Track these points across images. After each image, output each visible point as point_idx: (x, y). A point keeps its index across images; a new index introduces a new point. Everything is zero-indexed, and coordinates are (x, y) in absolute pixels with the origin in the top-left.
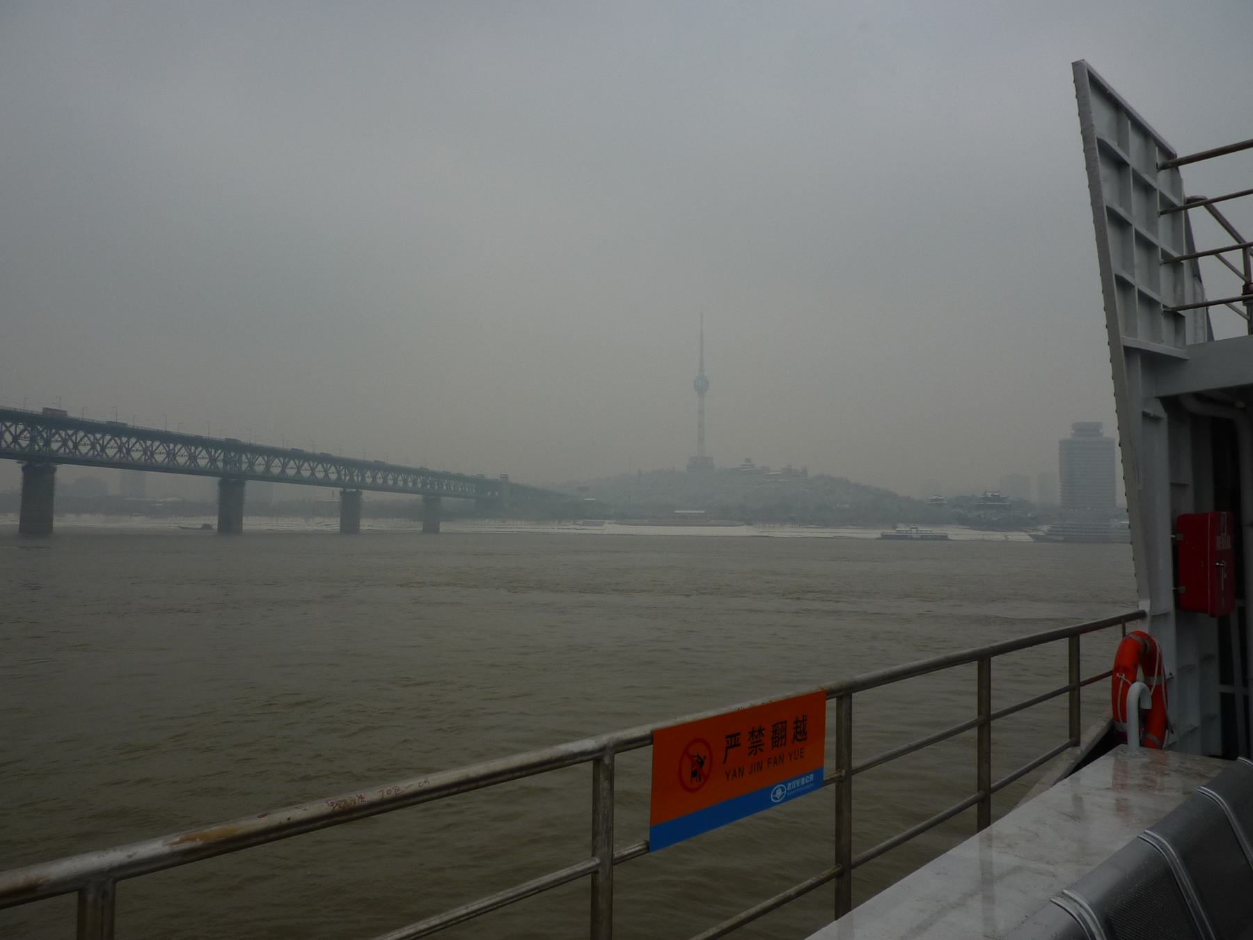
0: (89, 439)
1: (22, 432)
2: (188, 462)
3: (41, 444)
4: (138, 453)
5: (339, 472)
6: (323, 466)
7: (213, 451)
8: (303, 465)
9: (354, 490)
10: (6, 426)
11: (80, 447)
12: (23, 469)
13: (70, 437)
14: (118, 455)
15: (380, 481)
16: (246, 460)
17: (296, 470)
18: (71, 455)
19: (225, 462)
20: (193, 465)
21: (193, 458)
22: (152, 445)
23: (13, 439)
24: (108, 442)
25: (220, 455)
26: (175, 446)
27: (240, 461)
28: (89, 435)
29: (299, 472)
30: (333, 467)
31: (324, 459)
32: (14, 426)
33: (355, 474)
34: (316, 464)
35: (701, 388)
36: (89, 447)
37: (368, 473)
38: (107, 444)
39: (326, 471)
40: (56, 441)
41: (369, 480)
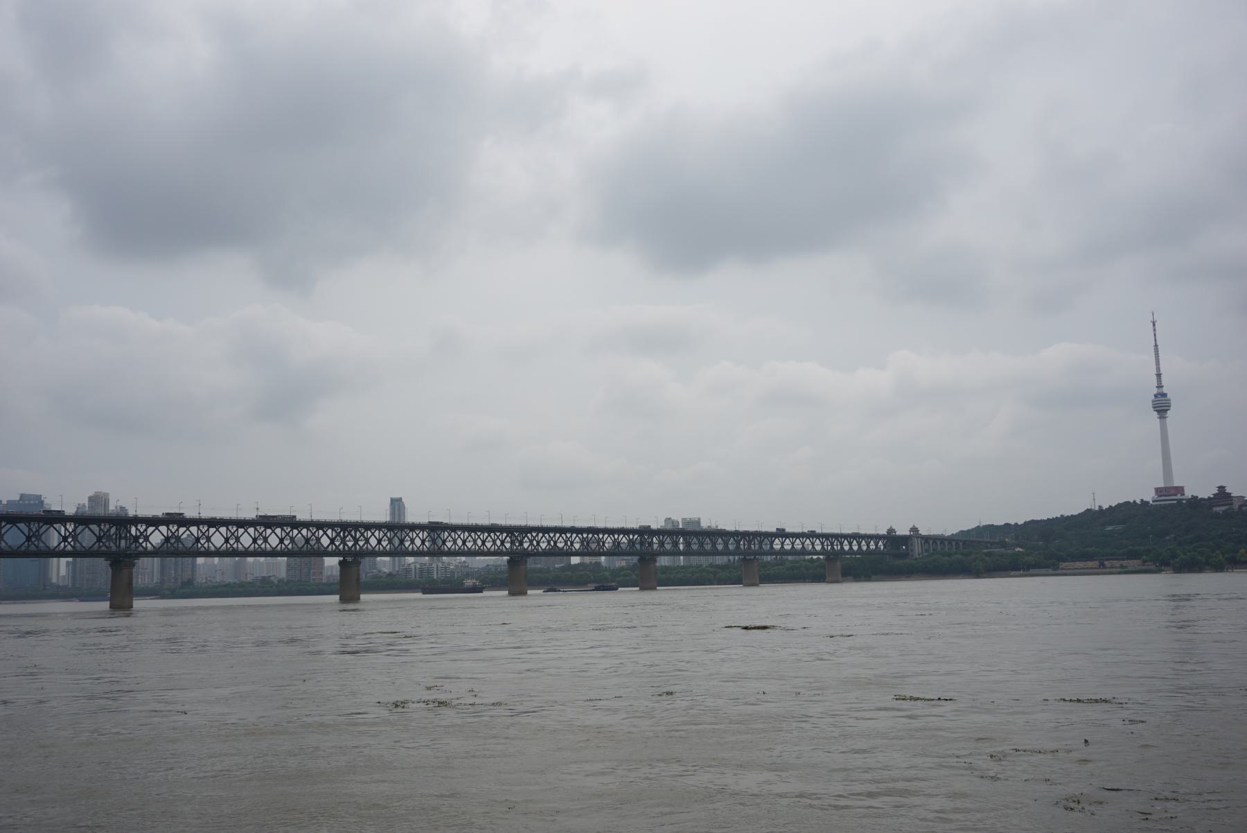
1: (487, 538)
3: (517, 544)
5: (822, 544)
8: (763, 540)
9: (752, 557)
11: (541, 544)
12: (111, 565)
13: (534, 538)
14: (27, 543)
15: (720, 547)
17: (791, 546)
18: (553, 551)
21: (701, 544)
22: (603, 538)
23: (97, 539)
26: (604, 535)
27: (651, 544)
29: (782, 547)
30: (798, 540)
31: (812, 535)
34: (784, 539)
35: (1161, 406)
36: (528, 544)
39: (813, 544)
40: (349, 541)
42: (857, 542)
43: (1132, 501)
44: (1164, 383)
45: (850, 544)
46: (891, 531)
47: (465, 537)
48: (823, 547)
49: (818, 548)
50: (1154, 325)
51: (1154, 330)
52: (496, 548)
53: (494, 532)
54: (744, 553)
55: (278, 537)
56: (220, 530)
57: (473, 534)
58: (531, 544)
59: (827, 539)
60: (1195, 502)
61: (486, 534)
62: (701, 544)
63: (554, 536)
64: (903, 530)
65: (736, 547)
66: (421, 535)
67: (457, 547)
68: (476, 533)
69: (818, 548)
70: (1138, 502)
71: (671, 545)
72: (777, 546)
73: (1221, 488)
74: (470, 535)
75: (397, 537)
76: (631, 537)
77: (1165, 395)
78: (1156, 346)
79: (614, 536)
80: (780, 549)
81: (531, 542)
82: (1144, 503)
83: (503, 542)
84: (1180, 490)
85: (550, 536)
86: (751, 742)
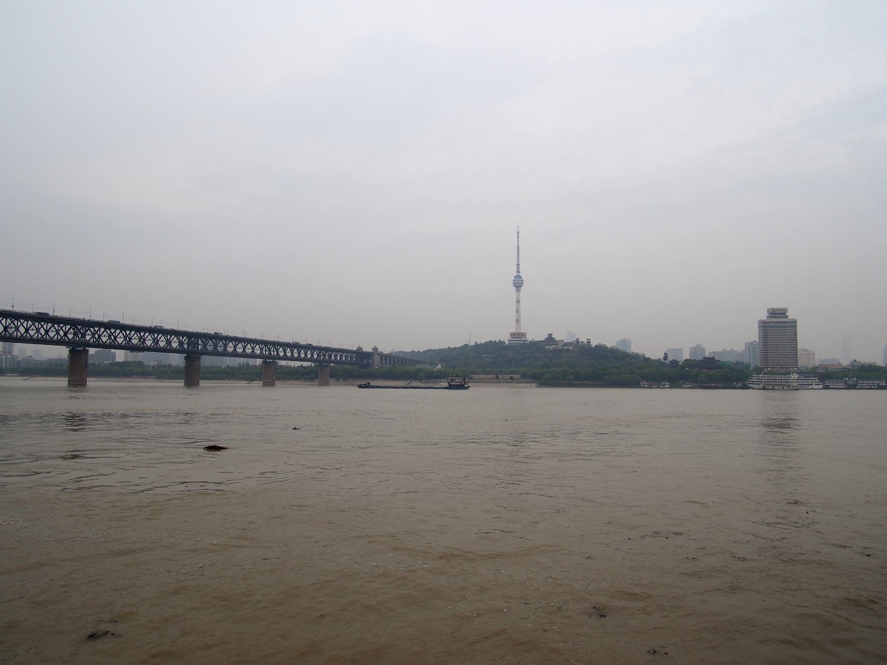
0: (107, 333)
1: (50, 328)
2: (166, 345)
3: (80, 336)
4: (53, 333)
5: (261, 349)
6: (222, 342)
7: (181, 337)
8: (238, 345)
10: (41, 324)
11: (30, 331)
13: (97, 332)
16: (202, 343)
19: (188, 344)
20: (169, 347)
22: (144, 335)
24: (119, 334)
25: (185, 340)
26: (130, 332)
28: (107, 330)
29: (244, 350)
32: (64, 327)
33: (272, 350)
35: (518, 284)
36: (35, 331)
37: (296, 351)
38: (50, 329)
41: (282, 354)
42: (283, 350)
43: (494, 341)
44: (521, 270)
45: (285, 351)
46: (84, 319)
47: (29, 326)
48: (262, 352)
49: (258, 352)
50: (518, 234)
51: (518, 237)
52: (95, 340)
53: (18, 320)
54: (321, 362)
55: (3, 326)
56: (55, 326)
57: (37, 324)
58: (93, 336)
59: (266, 345)
60: (534, 344)
61: (30, 323)
62: (215, 346)
63: (115, 332)
64: (367, 349)
65: (234, 350)
66: (25, 324)
67: (59, 337)
68: (39, 323)
69: (258, 352)
70: (497, 341)
71: (212, 347)
72: (230, 349)
73: (550, 335)
74: (13, 322)
75: (23, 326)
76: (156, 335)
77: (520, 277)
78: (518, 247)
79: (140, 334)
80: (242, 353)
81: (93, 335)
82: (501, 343)
83: (66, 334)
84: (524, 334)
85: (94, 330)
86: (278, 505)
